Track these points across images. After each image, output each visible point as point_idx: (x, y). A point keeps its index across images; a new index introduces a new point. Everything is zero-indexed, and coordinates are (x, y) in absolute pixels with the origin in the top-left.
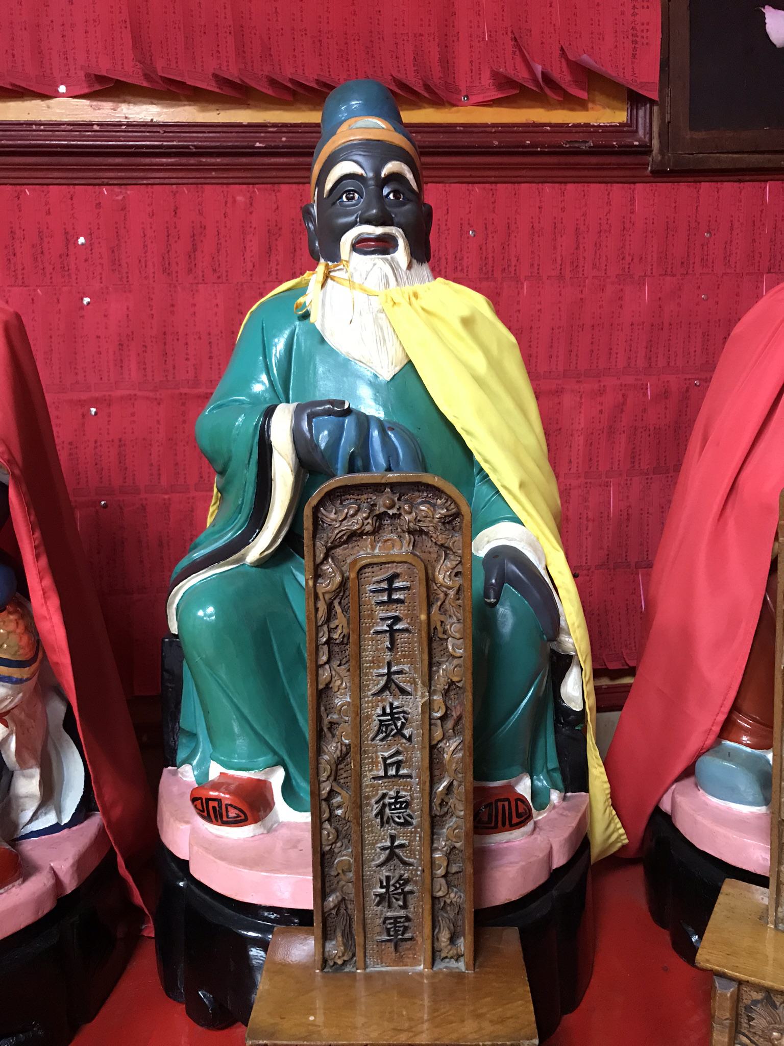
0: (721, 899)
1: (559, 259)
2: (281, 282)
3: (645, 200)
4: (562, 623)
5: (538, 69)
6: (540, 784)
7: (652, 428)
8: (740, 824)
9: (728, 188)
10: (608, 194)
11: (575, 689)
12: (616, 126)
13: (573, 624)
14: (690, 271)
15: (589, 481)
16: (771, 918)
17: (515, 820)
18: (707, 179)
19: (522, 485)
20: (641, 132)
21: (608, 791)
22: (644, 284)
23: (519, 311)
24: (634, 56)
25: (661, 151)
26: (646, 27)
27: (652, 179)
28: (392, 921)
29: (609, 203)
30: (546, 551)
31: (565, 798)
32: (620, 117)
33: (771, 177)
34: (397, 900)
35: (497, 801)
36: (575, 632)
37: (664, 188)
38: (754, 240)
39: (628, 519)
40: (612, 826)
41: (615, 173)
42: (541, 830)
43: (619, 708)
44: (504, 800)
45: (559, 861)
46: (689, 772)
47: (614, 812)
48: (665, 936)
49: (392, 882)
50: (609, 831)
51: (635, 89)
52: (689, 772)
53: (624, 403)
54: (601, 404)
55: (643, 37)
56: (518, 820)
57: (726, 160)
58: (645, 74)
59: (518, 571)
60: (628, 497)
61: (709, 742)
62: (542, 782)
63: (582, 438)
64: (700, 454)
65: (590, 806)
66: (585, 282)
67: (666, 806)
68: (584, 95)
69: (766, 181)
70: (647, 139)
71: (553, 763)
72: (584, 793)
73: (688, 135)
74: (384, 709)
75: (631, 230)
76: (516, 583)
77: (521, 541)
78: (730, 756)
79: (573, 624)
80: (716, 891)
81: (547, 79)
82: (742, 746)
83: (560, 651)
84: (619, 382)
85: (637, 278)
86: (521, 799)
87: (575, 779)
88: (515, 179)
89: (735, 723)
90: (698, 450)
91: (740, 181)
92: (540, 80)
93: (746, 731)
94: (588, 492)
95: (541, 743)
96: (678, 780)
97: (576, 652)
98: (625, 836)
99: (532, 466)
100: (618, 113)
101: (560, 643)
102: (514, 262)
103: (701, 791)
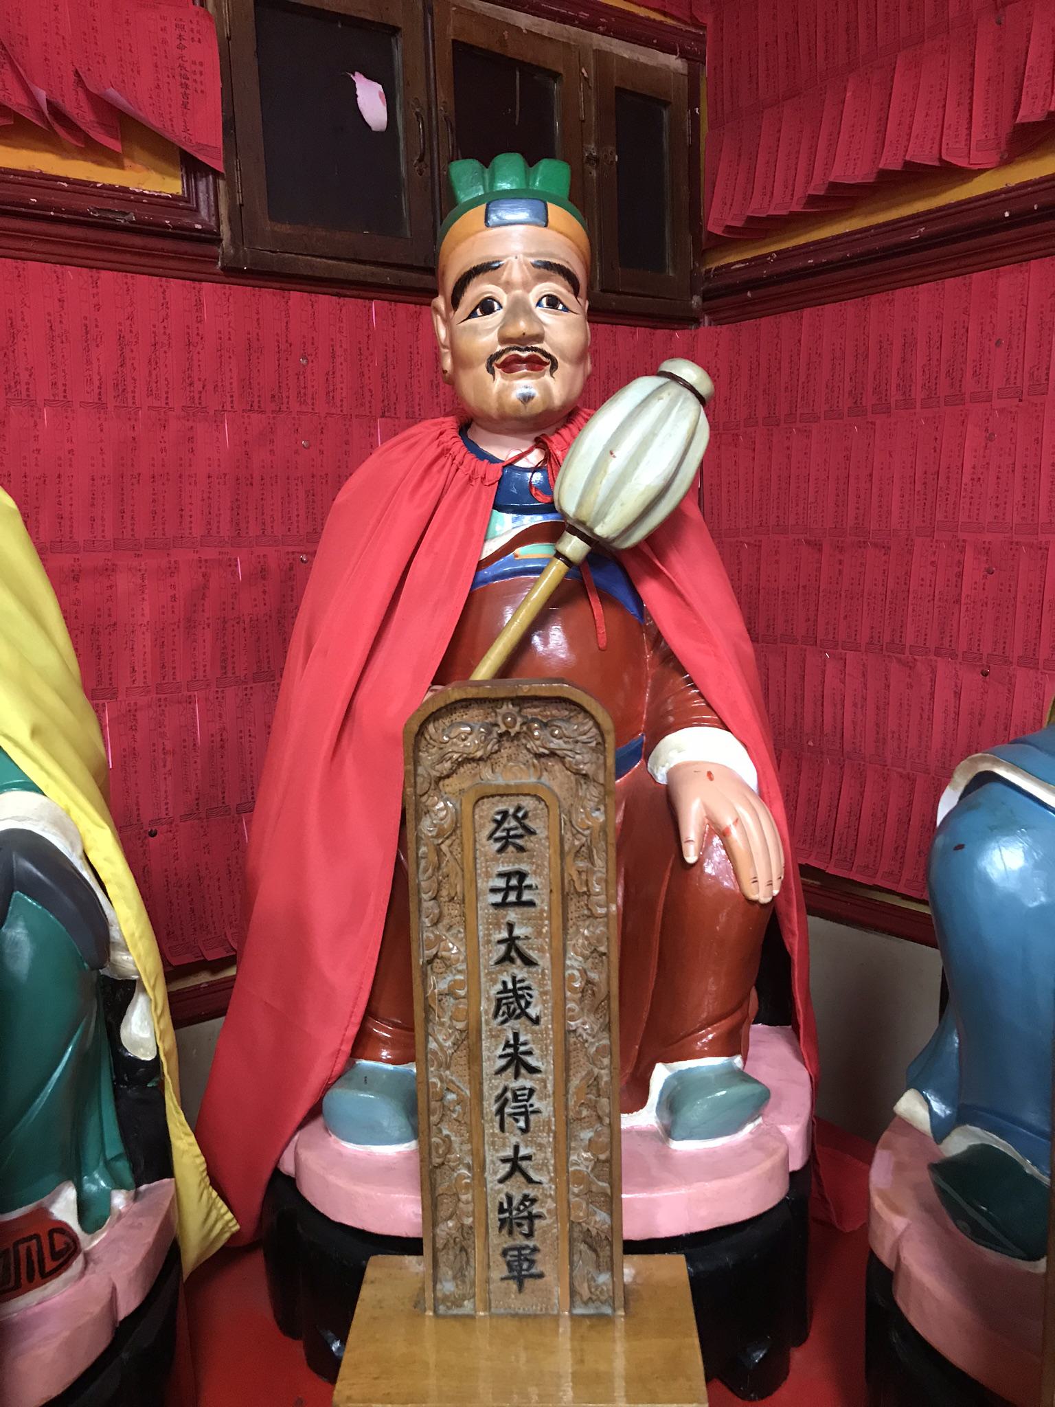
0: (366, 1292)
1: (96, 378)
2: (399, 172)
3: (218, 307)
4: (114, 934)
5: (42, 95)
6: (94, 1188)
7: (247, 620)
8: (384, 1173)
9: (325, 302)
10: (164, 292)
11: (143, 1030)
12: (167, 198)
13: (133, 935)
14: (284, 407)
15: (163, 696)
16: (429, 1302)
17: (50, 1265)
18: (298, 287)
19: (35, 732)
20: (204, 213)
21: (205, 1166)
22: (222, 422)
23: (38, 451)
24: (185, 105)
25: (233, 241)
26: (198, 68)
27: (224, 279)
28: (516, 1253)
29: (165, 305)
30: (81, 829)
31: (136, 1197)
32: (171, 185)
33: (378, 295)
34: (520, 1225)
35: (16, 1244)
36: (135, 946)
37: (241, 294)
38: (362, 374)
39: (222, 747)
40: (214, 1214)
41: (172, 264)
42: (96, 1263)
43: (221, 1012)
44: (30, 1238)
45: (127, 1305)
46: (316, 1111)
47: (215, 1194)
48: (297, 1349)
49: (515, 1203)
50: (206, 1218)
51: (188, 150)
52: (316, 1111)
53: (205, 587)
54: (173, 586)
55: (195, 81)
56: (57, 1263)
57: (322, 266)
58: (204, 132)
59: (34, 870)
60: (220, 716)
61: (338, 1068)
62: (97, 1183)
63: (148, 636)
64: (304, 668)
65: (176, 1200)
66: (136, 413)
67: (288, 1167)
68: (115, 145)
69: (372, 299)
70: (213, 224)
71: (114, 1147)
72: (166, 1180)
73: (268, 226)
74: (504, 983)
75: (200, 347)
76: (32, 888)
77: (40, 818)
78: (366, 1082)
79: (133, 935)
80: (361, 1272)
81: (57, 113)
82: (380, 1064)
83: (116, 977)
84: (196, 556)
85: (212, 413)
86: (63, 1228)
87: (152, 1161)
88: (17, 253)
89: (371, 1033)
90: (301, 661)
91: (339, 295)
92: (46, 112)
93: (385, 1042)
94: (163, 714)
95: (93, 1123)
96: (301, 1126)
97: (138, 974)
98: (234, 1221)
99: (52, 700)
100: (168, 180)
101: (114, 966)
102: (24, 376)
103: (333, 1137)
